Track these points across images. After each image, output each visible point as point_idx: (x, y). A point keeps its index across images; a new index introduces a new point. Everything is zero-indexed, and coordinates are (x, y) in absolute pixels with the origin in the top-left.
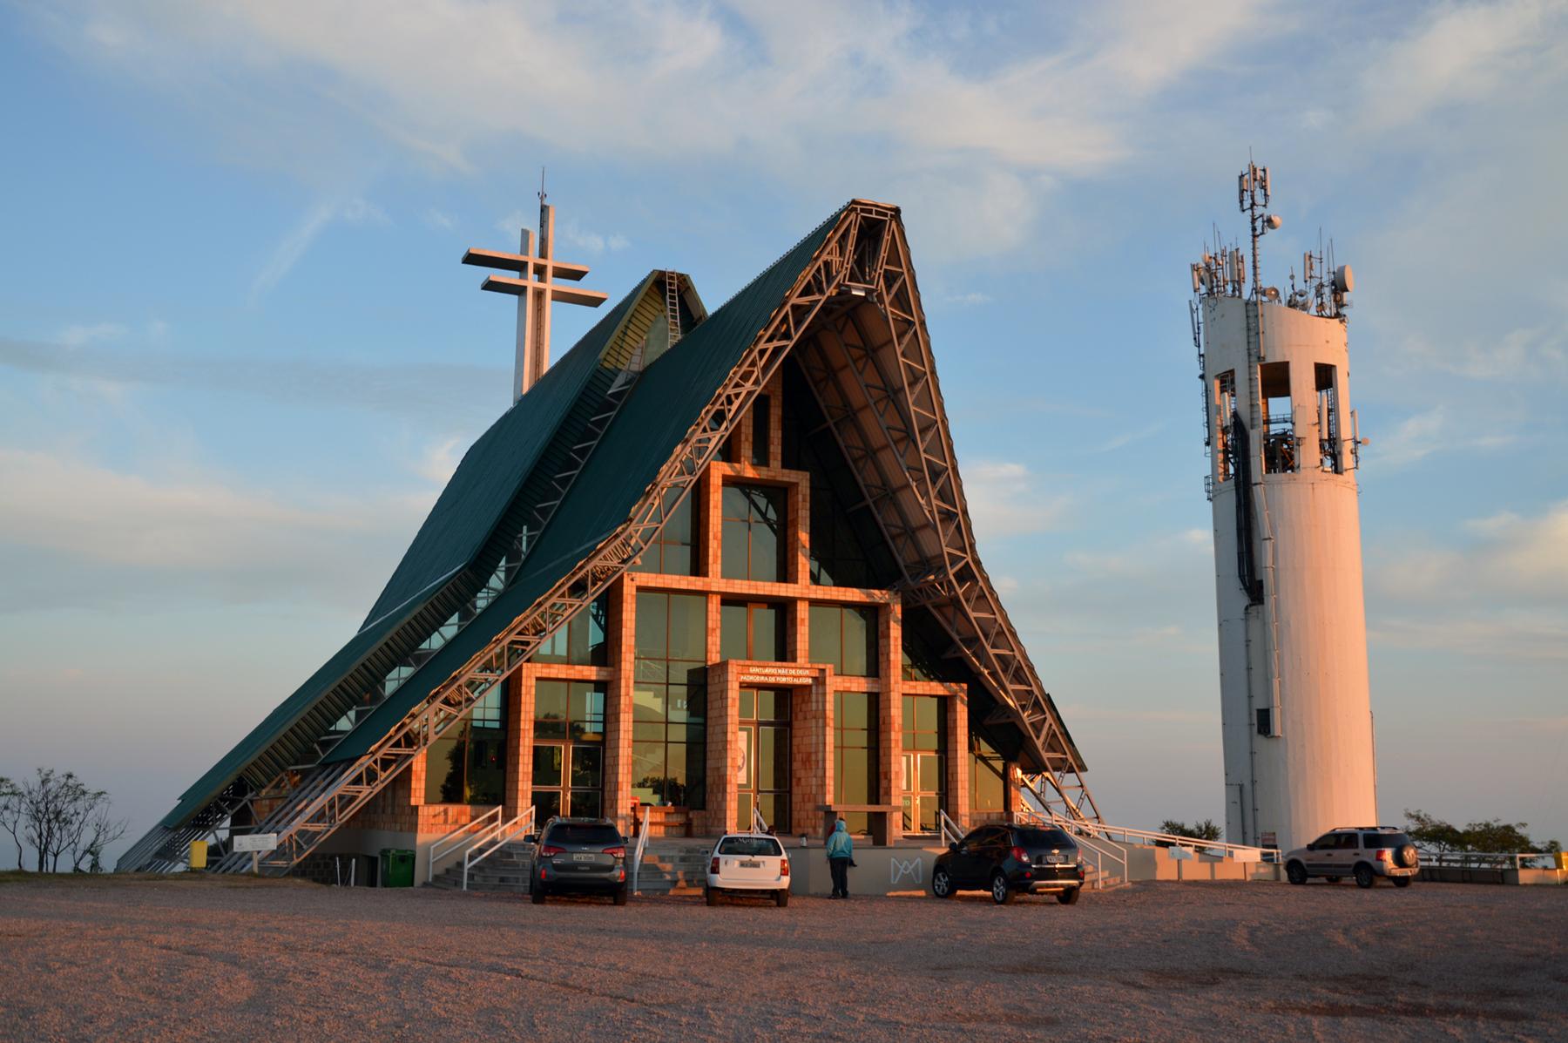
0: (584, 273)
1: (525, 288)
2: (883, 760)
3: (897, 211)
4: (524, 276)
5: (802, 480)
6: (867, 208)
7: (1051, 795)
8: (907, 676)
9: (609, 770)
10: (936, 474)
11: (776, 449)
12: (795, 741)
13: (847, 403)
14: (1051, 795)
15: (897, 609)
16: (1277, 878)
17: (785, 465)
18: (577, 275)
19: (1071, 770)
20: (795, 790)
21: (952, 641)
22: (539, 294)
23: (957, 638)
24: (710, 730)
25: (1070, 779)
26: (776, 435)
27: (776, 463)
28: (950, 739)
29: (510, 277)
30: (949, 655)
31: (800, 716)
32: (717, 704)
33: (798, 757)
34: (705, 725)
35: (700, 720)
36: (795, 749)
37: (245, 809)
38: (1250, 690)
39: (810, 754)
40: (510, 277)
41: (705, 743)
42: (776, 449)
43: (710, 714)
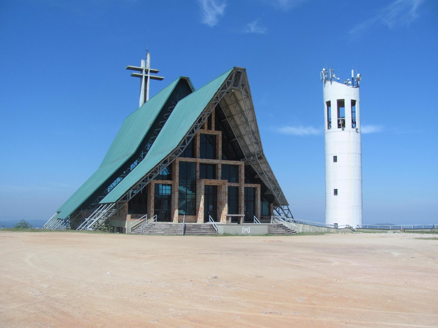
0: (163, 79)
1: (142, 76)
2: (239, 203)
3: (245, 70)
4: (142, 73)
5: (219, 134)
6: (238, 69)
7: (281, 211)
8: (246, 182)
9: (172, 206)
10: (253, 133)
11: (213, 125)
12: (218, 199)
13: (240, 132)
14: (281, 211)
15: (243, 166)
16: (170, 185)
17: (216, 129)
18: (156, 72)
19: (286, 205)
20: (218, 210)
21: (257, 174)
22: (146, 78)
23: (258, 173)
24: (197, 196)
25: (285, 207)
26: (213, 122)
27: (213, 129)
28: (256, 198)
29: (138, 73)
30: (256, 177)
31: (219, 192)
32: (199, 190)
33: (219, 203)
34: (196, 195)
35: (195, 193)
36: (218, 201)
37: (81, 215)
38: (257, 235)
39: (222, 202)
40: (138, 73)
41: (196, 199)
42: (213, 125)
43: (197, 192)
